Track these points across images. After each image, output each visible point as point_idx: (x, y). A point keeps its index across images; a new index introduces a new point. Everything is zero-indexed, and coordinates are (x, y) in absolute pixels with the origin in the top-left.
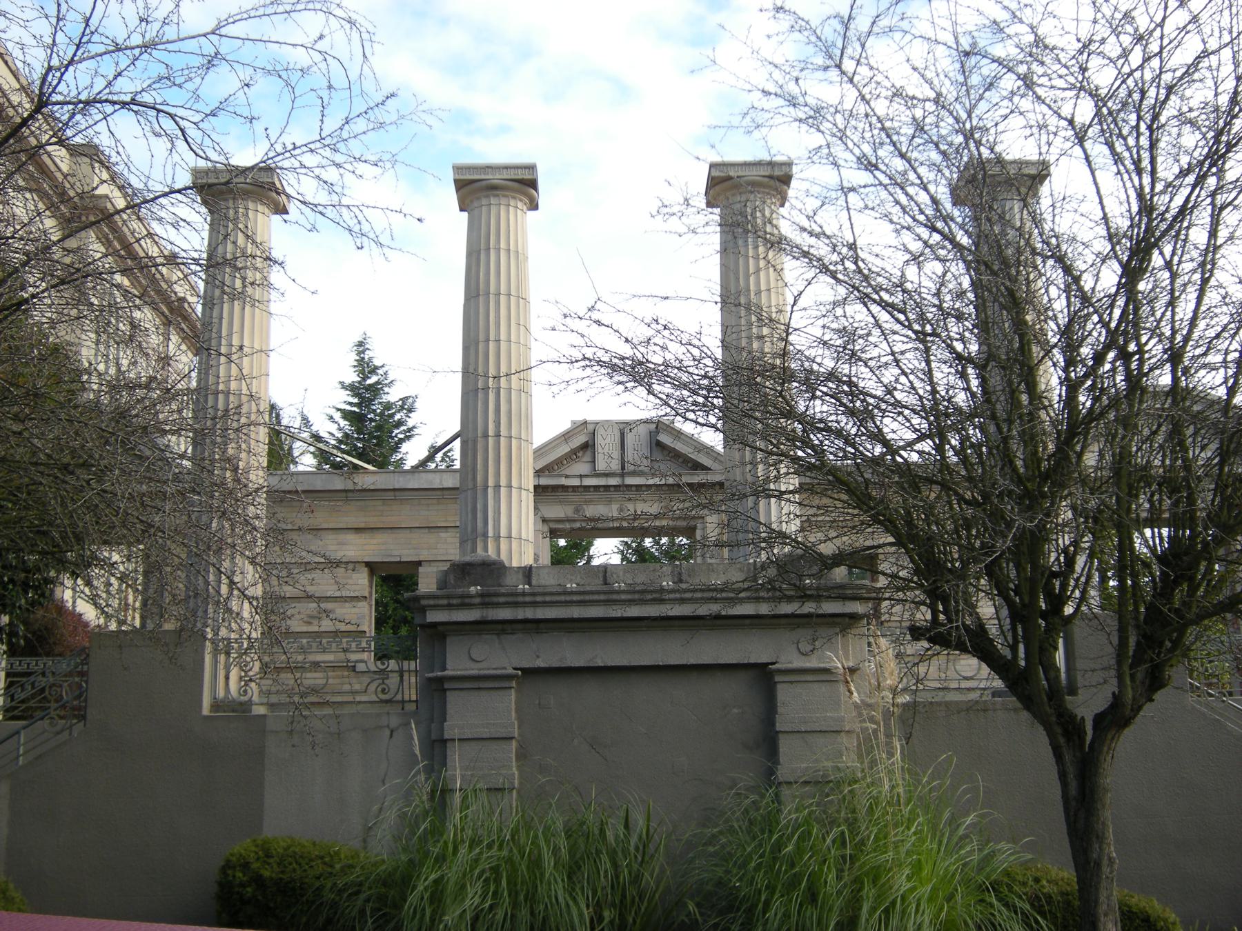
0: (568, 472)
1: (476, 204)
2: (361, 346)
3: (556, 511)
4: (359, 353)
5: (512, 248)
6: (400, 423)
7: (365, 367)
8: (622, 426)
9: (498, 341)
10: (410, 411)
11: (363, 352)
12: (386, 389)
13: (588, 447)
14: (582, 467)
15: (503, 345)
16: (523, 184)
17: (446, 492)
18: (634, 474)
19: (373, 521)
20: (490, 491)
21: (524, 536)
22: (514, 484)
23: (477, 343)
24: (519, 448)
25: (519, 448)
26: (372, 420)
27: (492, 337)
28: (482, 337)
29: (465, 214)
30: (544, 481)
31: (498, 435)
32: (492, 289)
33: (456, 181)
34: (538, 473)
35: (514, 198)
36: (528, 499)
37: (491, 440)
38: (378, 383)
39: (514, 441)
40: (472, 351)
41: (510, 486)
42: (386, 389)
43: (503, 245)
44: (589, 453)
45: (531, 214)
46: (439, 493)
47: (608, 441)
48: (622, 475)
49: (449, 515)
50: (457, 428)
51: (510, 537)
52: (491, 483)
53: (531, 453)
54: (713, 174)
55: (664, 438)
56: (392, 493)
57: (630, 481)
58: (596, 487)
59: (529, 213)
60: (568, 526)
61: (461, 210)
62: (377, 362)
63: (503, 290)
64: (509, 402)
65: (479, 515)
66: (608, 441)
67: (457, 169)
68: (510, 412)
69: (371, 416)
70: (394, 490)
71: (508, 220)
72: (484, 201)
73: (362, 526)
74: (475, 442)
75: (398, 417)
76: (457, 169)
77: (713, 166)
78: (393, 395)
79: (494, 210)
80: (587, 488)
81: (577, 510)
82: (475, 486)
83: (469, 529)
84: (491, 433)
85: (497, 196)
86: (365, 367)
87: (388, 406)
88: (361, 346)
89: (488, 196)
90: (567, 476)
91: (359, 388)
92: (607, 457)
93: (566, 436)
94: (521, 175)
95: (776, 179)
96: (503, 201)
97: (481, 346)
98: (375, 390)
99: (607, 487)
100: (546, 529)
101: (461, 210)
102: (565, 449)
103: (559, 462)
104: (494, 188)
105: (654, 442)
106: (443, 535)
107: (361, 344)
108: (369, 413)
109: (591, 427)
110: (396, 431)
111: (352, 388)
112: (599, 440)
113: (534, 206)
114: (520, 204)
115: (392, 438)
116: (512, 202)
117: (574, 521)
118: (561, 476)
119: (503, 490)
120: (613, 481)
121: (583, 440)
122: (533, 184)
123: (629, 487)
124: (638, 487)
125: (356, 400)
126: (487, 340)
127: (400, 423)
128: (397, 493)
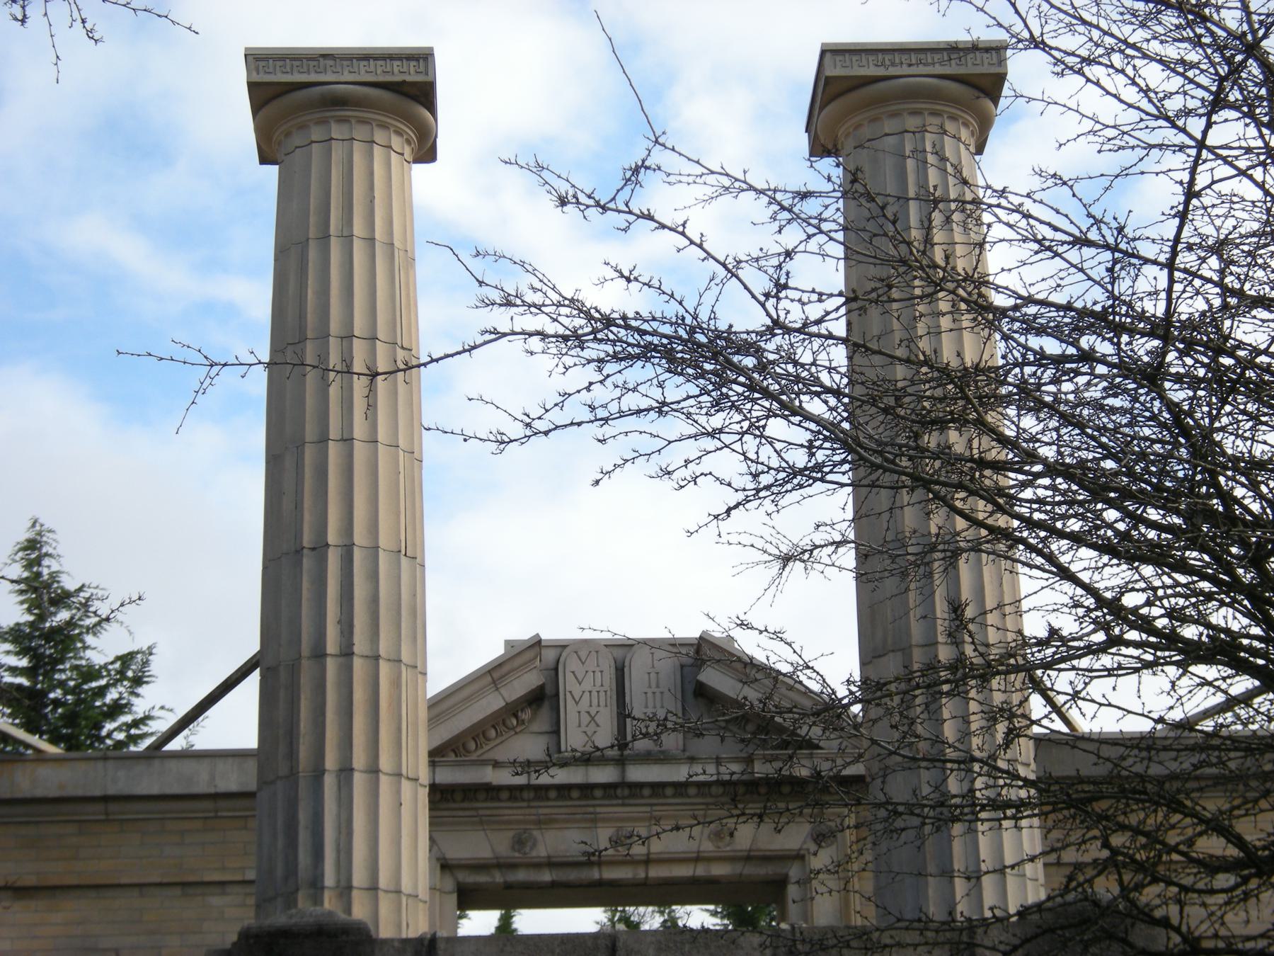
0: (502, 754)
1: (297, 140)
2: (34, 549)
3: (474, 845)
4: (29, 565)
5: (378, 235)
6: (117, 709)
7: (41, 590)
8: (619, 653)
9: (348, 440)
10: (138, 681)
11: (38, 562)
12: (89, 639)
13: (544, 698)
14: (529, 746)
15: (360, 450)
16: (398, 94)
17: (222, 804)
18: (647, 758)
19: (55, 871)
20: (329, 781)
21: (406, 886)
22: (385, 763)
23: (300, 446)
24: (396, 683)
25: (396, 683)
26: (56, 703)
27: (334, 431)
28: (310, 432)
29: (274, 169)
30: (447, 776)
31: (347, 653)
32: (335, 327)
33: (253, 87)
34: (437, 756)
35: (384, 126)
36: (415, 803)
37: (331, 666)
38: (70, 623)
39: (384, 668)
40: (289, 462)
41: (374, 771)
42: (89, 639)
43: (358, 229)
44: (545, 712)
45: (419, 170)
46: (207, 804)
47: (587, 685)
48: (621, 762)
49: (235, 854)
50: (252, 645)
51: (373, 888)
52: (331, 762)
53: (423, 714)
54: (830, 72)
55: (712, 677)
56: (99, 807)
57: (638, 774)
58: (564, 790)
59: (417, 168)
60: (498, 877)
61: (264, 160)
62: (70, 584)
63: (359, 327)
64: (374, 576)
65: (304, 837)
66: (587, 685)
67: (255, 58)
68: (374, 600)
69: (56, 694)
70: (106, 799)
71: (371, 174)
72: (316, 133)
73: (30, 881)
74: (294, 669)
75: (112, 695)
76: (255, 58)
77: (828, 52)
78: (102, 649)
79: (337, 151)
80: (541, 791)
81: (519, 843)
82: (293, 774)
83: (280, 871)
84: (332, 646)
85: (343, 120)
86: (41, 590)
87: (90, 673)
88: (34, 549)
89: (324, 122)
90: (496, 764)
91: (31, 637)
92: (586, 719)
93: (494, 674)
94: (397, 73)
95: (966, 84)
96: (360, 132)
97: (309, 453)
98: (65, 639)
99: (586, 790)
100: (449, 884)
101: (264, 160)
102: (493, 703)
103: (478, 733)
104: (338, 102)
105: (690, 688)
106: (216, 901)
107: (32, 545)
108: (53, 689)
109: (549, 656)
110: (109, 726)
111: (16, 635)
112: (569, 684)
113: (426, 153)
114: (396, 142)
115: (101, 740)
116: (379, 136)
117: (513, 866)
118: (484, 763)
119: (359, 780)
120: (602, 775)
121: (533, 681)
122: (424, 94)
123: (638, 786)
124: (657, 788)
125: (24, 663)
126: (323, 440)
127: (117, 709)
128: (113, 807)
